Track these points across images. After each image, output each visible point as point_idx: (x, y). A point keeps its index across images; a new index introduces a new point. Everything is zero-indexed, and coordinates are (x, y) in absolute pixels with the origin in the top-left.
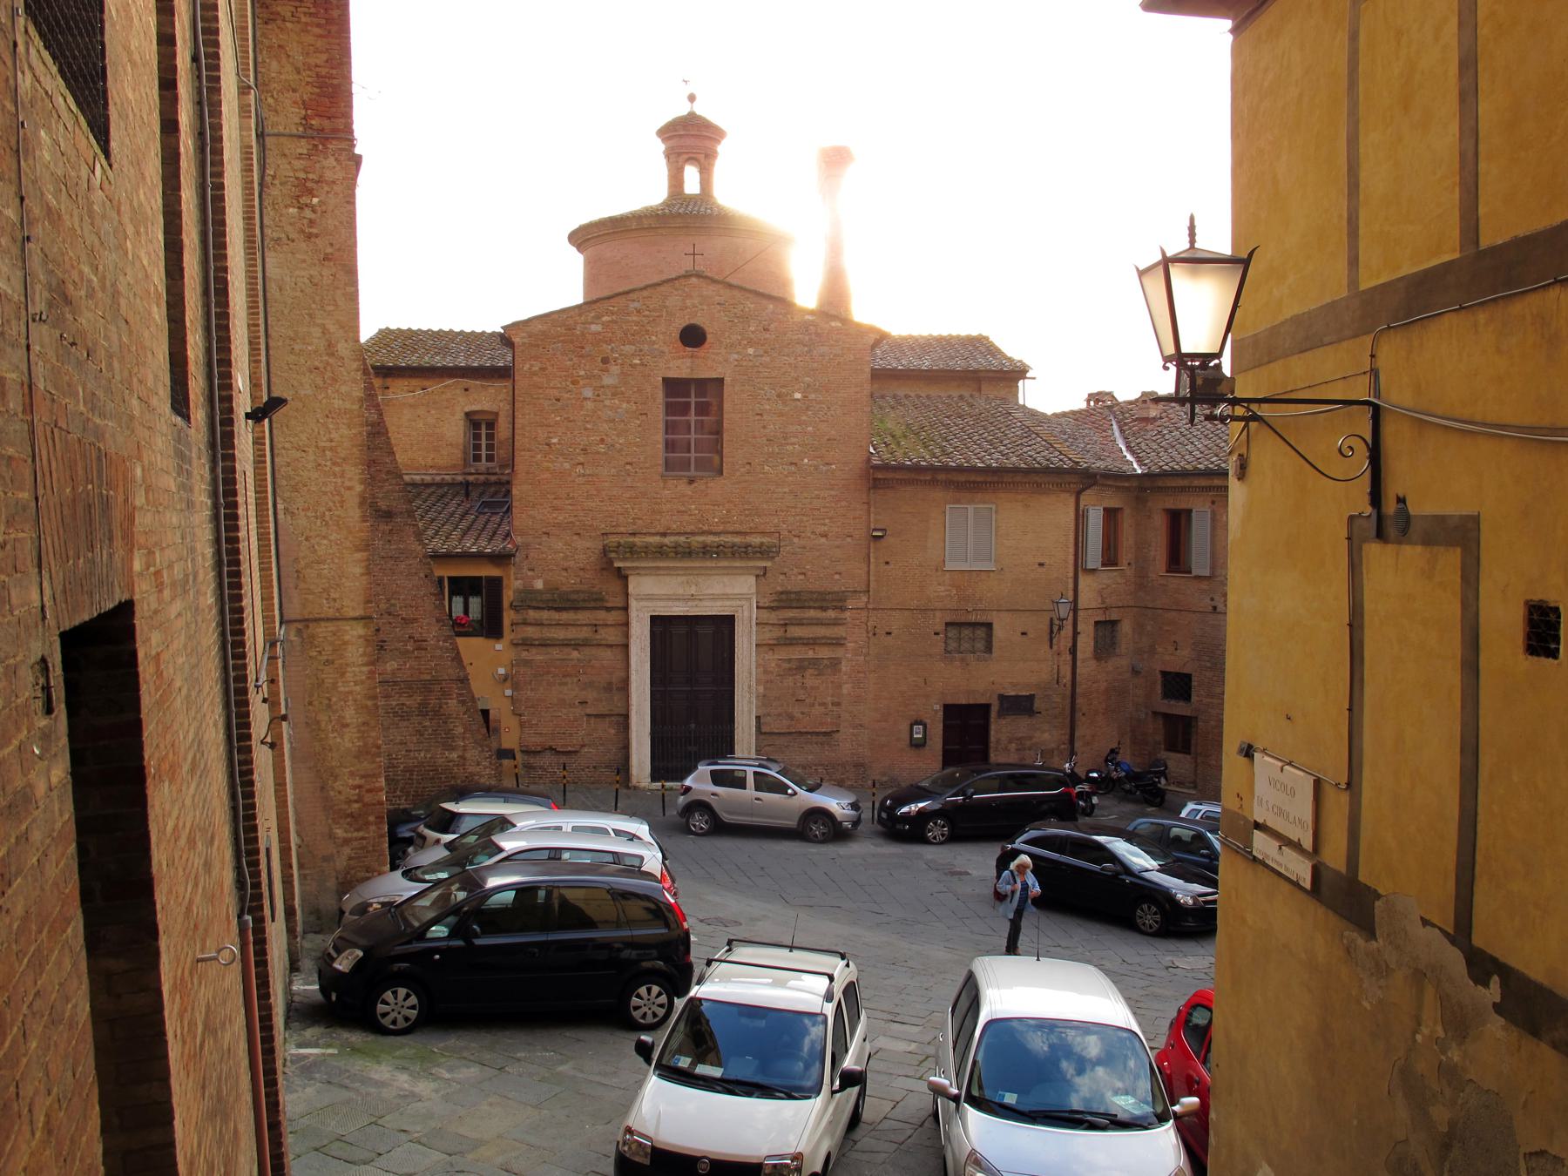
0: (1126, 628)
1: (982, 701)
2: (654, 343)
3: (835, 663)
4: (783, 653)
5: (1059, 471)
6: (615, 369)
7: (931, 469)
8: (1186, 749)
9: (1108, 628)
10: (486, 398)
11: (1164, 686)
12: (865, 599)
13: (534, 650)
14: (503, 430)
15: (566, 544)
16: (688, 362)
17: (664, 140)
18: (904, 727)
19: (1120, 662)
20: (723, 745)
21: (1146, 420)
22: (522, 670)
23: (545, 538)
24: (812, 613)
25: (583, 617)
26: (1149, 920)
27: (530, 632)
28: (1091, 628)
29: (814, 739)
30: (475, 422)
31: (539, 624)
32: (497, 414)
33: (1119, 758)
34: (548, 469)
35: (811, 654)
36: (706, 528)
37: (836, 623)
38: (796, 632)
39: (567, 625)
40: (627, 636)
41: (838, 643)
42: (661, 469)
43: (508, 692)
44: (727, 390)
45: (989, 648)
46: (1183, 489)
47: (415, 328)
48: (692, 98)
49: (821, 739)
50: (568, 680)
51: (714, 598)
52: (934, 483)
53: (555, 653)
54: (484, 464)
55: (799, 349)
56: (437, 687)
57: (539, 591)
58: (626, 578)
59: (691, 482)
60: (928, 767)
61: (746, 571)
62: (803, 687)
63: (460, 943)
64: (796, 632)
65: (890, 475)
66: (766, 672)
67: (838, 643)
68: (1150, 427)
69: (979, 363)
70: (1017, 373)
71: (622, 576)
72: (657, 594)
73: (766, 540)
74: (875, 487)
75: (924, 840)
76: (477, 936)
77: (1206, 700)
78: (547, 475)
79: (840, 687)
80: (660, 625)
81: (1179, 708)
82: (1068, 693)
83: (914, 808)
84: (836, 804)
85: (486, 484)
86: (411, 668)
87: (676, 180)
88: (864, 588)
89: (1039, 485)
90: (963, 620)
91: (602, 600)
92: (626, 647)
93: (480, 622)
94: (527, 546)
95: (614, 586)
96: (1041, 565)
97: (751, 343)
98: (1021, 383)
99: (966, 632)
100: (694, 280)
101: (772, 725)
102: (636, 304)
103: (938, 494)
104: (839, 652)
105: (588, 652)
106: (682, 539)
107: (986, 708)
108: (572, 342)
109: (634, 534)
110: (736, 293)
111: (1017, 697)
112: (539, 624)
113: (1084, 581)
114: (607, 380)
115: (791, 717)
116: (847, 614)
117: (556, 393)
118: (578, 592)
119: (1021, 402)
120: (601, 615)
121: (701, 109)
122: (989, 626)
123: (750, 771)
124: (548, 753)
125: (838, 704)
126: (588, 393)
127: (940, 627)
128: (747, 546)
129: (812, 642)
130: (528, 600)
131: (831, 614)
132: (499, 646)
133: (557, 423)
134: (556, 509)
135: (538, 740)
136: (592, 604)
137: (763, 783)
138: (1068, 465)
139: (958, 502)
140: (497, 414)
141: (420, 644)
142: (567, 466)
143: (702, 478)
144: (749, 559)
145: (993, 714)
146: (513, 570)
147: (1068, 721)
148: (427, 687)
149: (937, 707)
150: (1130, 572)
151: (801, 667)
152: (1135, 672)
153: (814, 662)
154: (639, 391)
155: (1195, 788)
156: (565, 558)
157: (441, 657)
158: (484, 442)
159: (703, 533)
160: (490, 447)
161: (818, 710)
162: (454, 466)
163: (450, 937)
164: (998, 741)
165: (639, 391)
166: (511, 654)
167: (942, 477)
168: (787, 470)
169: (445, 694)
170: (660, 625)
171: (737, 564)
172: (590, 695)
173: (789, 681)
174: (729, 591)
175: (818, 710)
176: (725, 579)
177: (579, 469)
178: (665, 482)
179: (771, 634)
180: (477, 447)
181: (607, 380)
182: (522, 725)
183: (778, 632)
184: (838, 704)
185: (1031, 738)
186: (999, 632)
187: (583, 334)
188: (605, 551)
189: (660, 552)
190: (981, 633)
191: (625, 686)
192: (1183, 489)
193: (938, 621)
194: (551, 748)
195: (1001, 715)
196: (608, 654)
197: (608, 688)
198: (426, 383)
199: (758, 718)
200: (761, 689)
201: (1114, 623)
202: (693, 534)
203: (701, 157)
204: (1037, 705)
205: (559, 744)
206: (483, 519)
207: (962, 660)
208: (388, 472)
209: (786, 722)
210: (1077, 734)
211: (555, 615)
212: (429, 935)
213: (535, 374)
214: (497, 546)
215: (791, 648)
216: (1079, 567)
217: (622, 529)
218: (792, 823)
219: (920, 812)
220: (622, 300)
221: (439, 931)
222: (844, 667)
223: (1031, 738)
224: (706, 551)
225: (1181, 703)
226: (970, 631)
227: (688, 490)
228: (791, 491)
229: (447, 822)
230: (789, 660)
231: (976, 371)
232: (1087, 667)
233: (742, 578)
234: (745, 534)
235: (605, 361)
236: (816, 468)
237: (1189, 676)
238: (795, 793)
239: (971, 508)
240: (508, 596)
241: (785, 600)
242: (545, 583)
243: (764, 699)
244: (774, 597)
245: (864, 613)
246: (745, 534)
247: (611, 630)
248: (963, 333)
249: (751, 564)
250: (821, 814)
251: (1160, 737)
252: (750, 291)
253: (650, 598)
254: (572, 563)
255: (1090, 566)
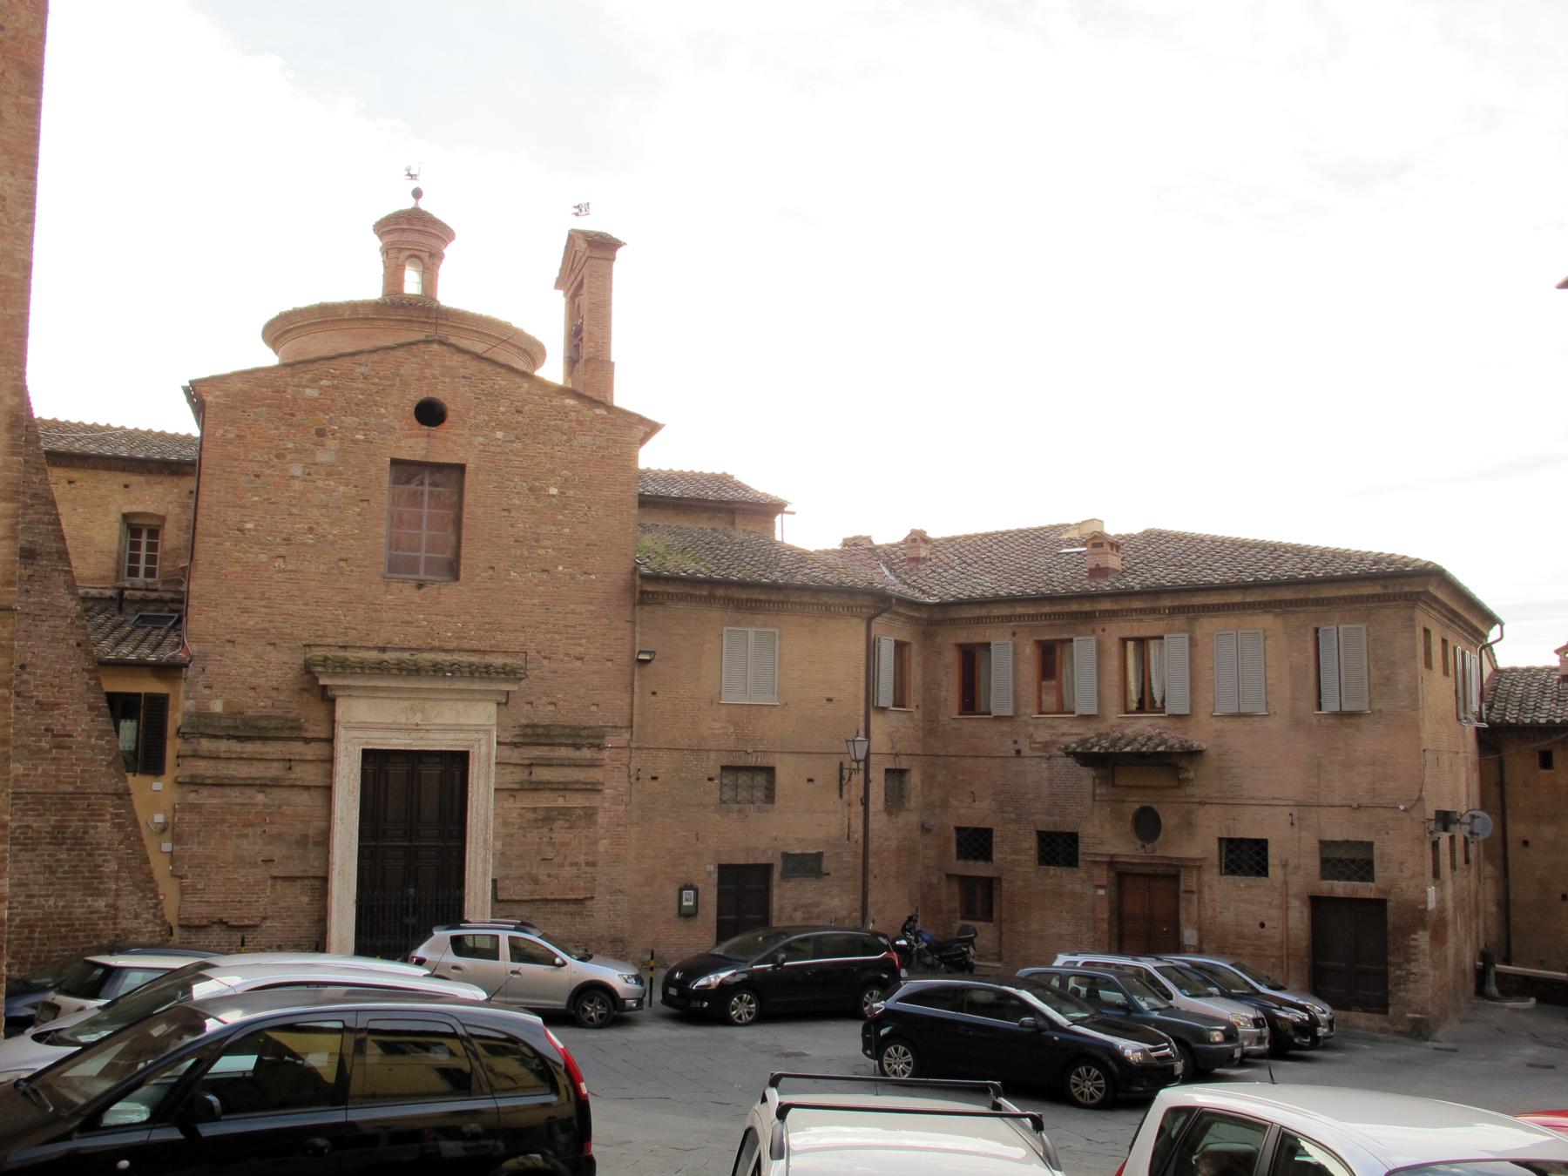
0: (915, 778)
1: (762, 860)
2: (383, 416)
3: (590, 814)
4: (526, 801)
5: (851, 592)
6: (332, 444)
7: (710, 582)
8: (988, 915)
9: (896, 775)
10: (152, 498)
11: (959, 843)
12: (627, 736)
13: (205, 792)
14: (171, 537)
15: (258, 656)
16: (423, 442)
17: (381, 235)
18: (672, 892)
19: (911, 817)
20: (453, 914)
21: (917, 560)
22: (187, 817)
23: (228, 647)
24: (563, 752)
25: (273, 749)
26: (1089, 1088)
27: (202, 767)
28: (882, 776)
29: (563, 908)
30: (134, 526)
31: (214, 757)
32: (163, 519)
33: (918, 926)
34: (238, 561)
35: (561, 803)
36: (436, 643)
37: (592, 765)
38: (543, 774)
39: (251, 759)
40: (330, 774)
41: (593, 789)
42: (383, 569)
43: (167, 847)
44: (469, 479)
45: (770, 797)
46: (979, 620)
47: (62, 419)
48: (417, 194)
49: (572, 908)
50: (250, 830)
51: (445, 729)
52: (710, 600)
53: (234, 795)
54: (141, 579)
55: (557, 436)
56: (82, 804)
57: (218, 715)
58: (332, 701)
59: (420, 586)
60: (701, 938)
61: (484, 695)
62: (551, 843)
63: (174, 1134)
64: (543, 774)
65: (660, 588)
66: (505, 824)
67: (593, 789)
68: (921, 567)
69: (729, 495)
70: (767, 510)
71: (328, 699)
72: (372, 721)
73: (509, 661)
74: (642, 602)
75: (727, 1021)
76: (211, 1116)
77: (1010, 858)
78: (238, 568)
79: (596, 843)
80: (371, 757)
81: (978, 869)
82: (860, 850)
83: (713, 979)
84: (617, 977)
85: (145, 602)
86: (45, 774)
87: (393, 277)
88: (626, 723)
89: (828, 607)
90: (741, 763)
91: (300, 728)
92: (328, 789)
93: (134, 753)
94: (204, 656)
95: (318, 712)
96: (829, 700)
97: (500, 426)
98: (778, 519)
99: (744, 778)
100: (435, 347)
101: (513, 891)
102: (363, 369)
103: (714, 614)
104: (595, 801)
105: (277, 795)
106: (406, 656)
107: (767, 869)
108: (279, 407)
109: (345, 647)
110: (485, 366)
111: (803, 855)
112: (214, 757)
113: (877, 721)
114: (323, 457)
115: (535, 881)
116: (606, 754)
117: (256, 467)
118: (267, 718)
119: (778, 537)
120: (297, 748)
121: (425, 205)
122: (770, 771)
123: (504, 937)
124: (216, 928)
125: (593, 864)
126: (297, 470)
127: (716, 772)
128: (487, 667)
129: (563, 788)
130: (202, 725)
131: (586, 753)
132: (157, 785)
133: (254, 505)
134: (245, 611)
135: (205, 910)
136: (286, 734)
137: (520, 953)
138: (862, 584)
139: (737, 623)
140: (163, 519)
141: (61, 740)
142: (263, 558)
143: (433, 582)
144: (492, 680)
145: (776, 875)
146: (183, 687)
147: (859, 884)
148: (66, 802)
149: (712, 868)
150: (918, 715)
151: (548, 818)
152: (925, 829)
153: (565, 812)
154: (361, 472)
155: (1000, 959)
156: (254, 674)
157: (92, 761)
158: (143, 553)
159: (432, 649)
160: (151, 560)
161: (568, 872)
162: (104, 578)
163: (156, 1118)
164: (781, 909)
165: (361, 472)
166: (174, 796)
167: (720, 592)
168: (536, 583)
169: (95, 814)
170: (371, 757)
171: (476, 686)
172: (277, 851)
173: (533, 836)
174: (463, 720)
175: (568, 872)
176: (460, 706)
177: (279, 563)
178: (388, 584)
179: (515, 777)
180: (134, 559)
181: (323, 457)
182: (183, 891)
183: (521, 775)
184: (593, 864)
185: (818, 904)
186: (781, 778)
187: (295, 399)
188: (308, 669)
189: (380, 669)
190: (760, 779)
191: (324, 840)
192: (979, 620)
193: (712, 764)
194: (221, 922)
195: (785, 876)
196: (304, 800)
197: (303, 841)
198: (74, 474)
199: (494, 881)
200: (499, 845)
201: (901, 772)
202: (419, 650)
203: (425, 255)
204: (826, 865)
205: (231, 915)
206: (140, 633)
207: (740, 811)
208: (34, 496)
209: (528, 887)
210: (870, 899)
211: (236, 747)
212: (109, 1120)
213: (230, 442)
214: (167, 654)
215: (536, 795)
216: (871, 703)
217: (330, 641)
218: (561, 1003)
219: (722, 984)
220: (346, 363)
221: (130, 1111)
222: (601, 819)
223: (818, 904)
224: (437, 670)
225: (980, 863)
226: (750, 777)
227: (416, 596)
228: (542, 604)
229: (95, 982)
230: (535, 810)
231: (729, 502)
232: (878, 821)
233: (480, 706)
234: (485, 652)
235: (321, 433)
236: (573, 577)
237: (989, 832)
238: (564, 964)
239: (751, 631)
240: (175, 719)
241: (532, 736)
242: (227, 704)
243: (502, 859)
244: (517, 731)
245: (626, 754)
246: (485, 652)
247: (309, 767)
248: (707, 471)
249: (493, 687)
250: (594, 990)
251: (956, 904)
252: (503, 366)
253: (364, 726)
254: (262, 681)
255: (881, 704)
